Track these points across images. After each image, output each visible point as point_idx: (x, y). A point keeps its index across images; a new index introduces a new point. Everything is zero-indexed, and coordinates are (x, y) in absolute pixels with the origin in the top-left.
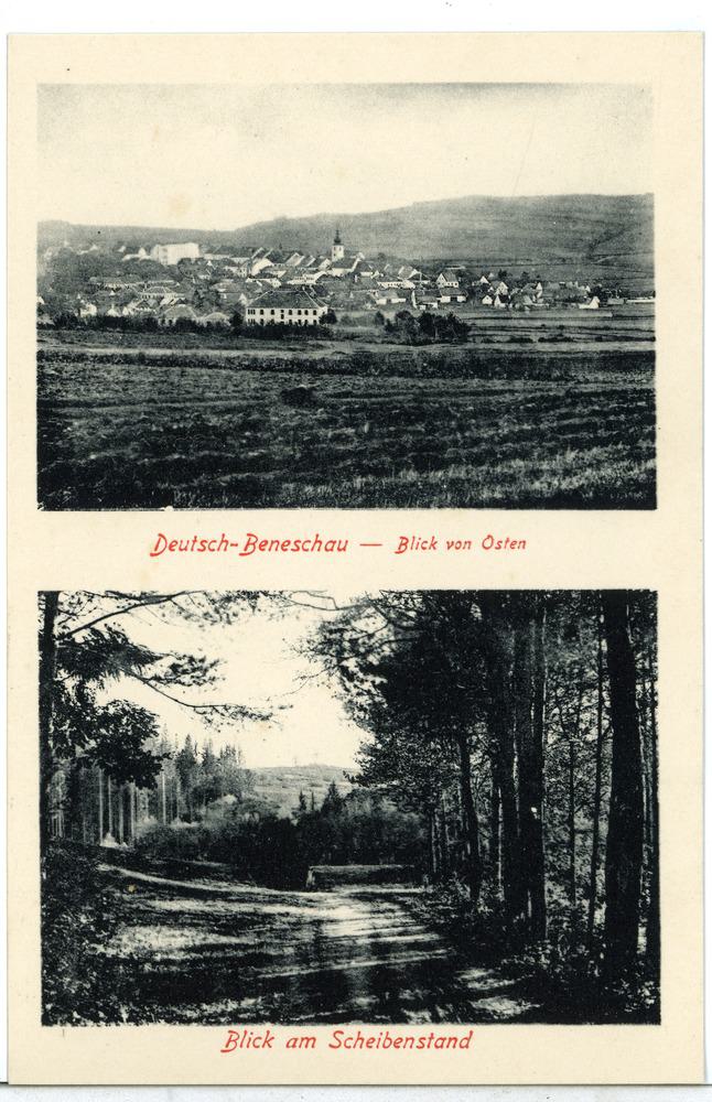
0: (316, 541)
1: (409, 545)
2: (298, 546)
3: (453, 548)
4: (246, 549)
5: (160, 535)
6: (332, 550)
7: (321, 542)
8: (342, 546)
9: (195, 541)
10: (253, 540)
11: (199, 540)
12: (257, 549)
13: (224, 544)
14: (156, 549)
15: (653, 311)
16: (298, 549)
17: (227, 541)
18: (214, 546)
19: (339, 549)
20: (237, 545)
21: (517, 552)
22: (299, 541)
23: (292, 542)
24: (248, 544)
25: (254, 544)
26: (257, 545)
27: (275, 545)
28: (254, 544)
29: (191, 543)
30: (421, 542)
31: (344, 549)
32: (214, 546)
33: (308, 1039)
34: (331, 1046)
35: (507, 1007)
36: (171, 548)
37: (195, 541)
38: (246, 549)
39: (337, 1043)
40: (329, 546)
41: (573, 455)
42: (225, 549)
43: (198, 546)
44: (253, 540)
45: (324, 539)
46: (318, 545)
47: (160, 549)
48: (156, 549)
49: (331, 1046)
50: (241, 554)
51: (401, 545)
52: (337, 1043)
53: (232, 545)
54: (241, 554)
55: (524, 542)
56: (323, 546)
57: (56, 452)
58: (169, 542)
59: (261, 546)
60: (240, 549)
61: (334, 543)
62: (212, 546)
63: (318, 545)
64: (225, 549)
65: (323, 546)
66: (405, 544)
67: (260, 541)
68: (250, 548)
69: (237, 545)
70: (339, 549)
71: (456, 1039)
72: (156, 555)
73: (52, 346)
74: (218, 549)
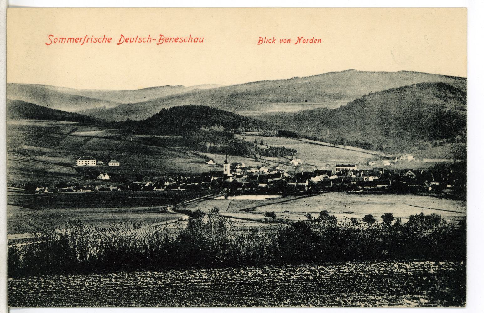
1: (263, 41)
2: (183, 40)
3: (283, 43)
5: (122, 35)
6: (197, 42)
7: (106, 38)
8: (201, 40)
9: (137, 38)
11: (139, 38)
14: (120, 41)
17: (151, 38)
20: (155, 40)
21: (318, 44)
22: (97, 38)
23: (180, 38)
24: (160, 39)
25: (163, 39)
26: (164, 40)
27: (172, 39)
29: (135, 39)
30: (268, 40)
31: (202, 41)
32: (145, 40)
35: (128, 93)
36: (283, 40)
37: (137, 38)
38: (159, 41)
39: (95, 41)
40: (196, 40)
42: (150, 42)
43: (138, 40)
45: (193, 37)
46: (191, 39)
48: (120, 41)
51: (260, 40)
52: (95, 41)
53: (153, 40)
54: (157, 44)
55: (321, 40)
56: (193, 39)
57: (57, 111)
58: (125, 39)
59: (166, 40)
61: (198, 38)
64: (150, 42)
65: (193, 39)
66: (262, 41)
67: (165, 38)
68: (161, 41)
69: (155, 40)
70: (200, 42)
71: (74, 39)
72: (160, 44)
73: (13, 237)
74: (188, 42)
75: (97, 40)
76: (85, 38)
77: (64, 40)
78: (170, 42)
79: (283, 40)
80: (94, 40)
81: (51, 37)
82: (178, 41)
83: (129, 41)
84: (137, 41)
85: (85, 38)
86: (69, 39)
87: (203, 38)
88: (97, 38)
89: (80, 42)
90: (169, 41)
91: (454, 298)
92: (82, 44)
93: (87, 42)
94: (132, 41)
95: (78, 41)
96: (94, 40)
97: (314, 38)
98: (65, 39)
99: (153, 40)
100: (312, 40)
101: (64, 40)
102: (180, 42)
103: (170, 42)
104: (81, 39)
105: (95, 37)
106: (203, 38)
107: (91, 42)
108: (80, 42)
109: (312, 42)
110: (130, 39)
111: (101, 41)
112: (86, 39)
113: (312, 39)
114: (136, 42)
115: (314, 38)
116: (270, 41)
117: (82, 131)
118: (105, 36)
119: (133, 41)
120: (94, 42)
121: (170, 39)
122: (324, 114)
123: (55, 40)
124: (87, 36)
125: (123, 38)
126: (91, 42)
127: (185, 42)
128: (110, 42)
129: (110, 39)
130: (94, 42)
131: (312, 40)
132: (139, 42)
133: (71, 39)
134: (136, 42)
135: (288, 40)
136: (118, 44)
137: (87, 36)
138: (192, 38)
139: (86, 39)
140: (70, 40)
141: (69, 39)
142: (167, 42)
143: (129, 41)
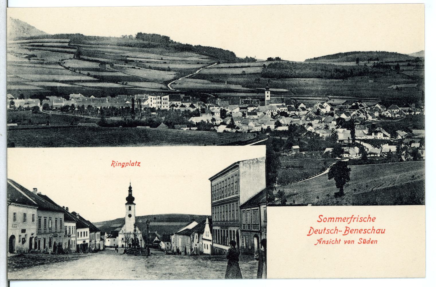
0: (369, 218)
4: (345, 233)
5: (311, 227)
6: (379, 233)
7: (371, 218)
8: (383, 232)
9: (325, 229)
10: (348, 229)
11: (327, 229)
12: (349, 232)
13: (336, 231)
14: (309, 232)
15: (424, 134)
16: (365, 230)
17: (337, 230)
18: (369, 231)
19: (382, 233)
20: (341, 231)
24: (346, 231)
25: (348, 231)
26: (349, 231)
28: (348, 231)
29: (323, 231)
31: (384, 233)
33: (331, 218)
34: (318, 221)
37: (325, 229)
38: (345, 233)
39: (320, 220)
40: (378, 231)
41: (143, 120)
42: (337, 233)
43: (326, 231)
44: (348, 229)
47: (310, 234)
48: (309, 232)
49: (318, 221)
50: (343, 235)
53: (339, 231)
54: (343, 235)
59: (351, 231)
60: (343, 233)
61: (380, 230)
62: (369, 231)
63: (337, 242)
64: (337, 233)
69: (341, 231)
71: (341, 218)
72: (345, 235)
75: (362, 219)
76: (351, 218)
77: (333, 219)
78: (354, 233)
79: (347, 241)
80: (359, 219)
81: (321, 217)
82: (362, 232)
83: (318, 232)
84: (325, 233)
85: (351, 218)
86: (337, 218)
87: (385, 230)
88: (362, 218)
89: (347, 221)
90: (353, 232)
91: (136, 247)
92: (348, 223)
93: (353, 221)
94: (320, 232)
95: (346, 220)
96: (359, 219)
97: (370, 239)
98: (334, 218)
99: (339, 231)
100: (369, 241)
101: (332, 219)
102: (364, 233)
103: (354, 233)
104: (348, 218)
105: (361, 217)
106: (385, 230)
107: (357, 221)
108: (347, 221)
109: (369, 243)
110: (319, 231)
111: (366, 221)
112: (353, 219)
113: (369, 240)
114: (324, 233)
115: (370, 239)
116: (333, 242)
117: (181, 229)
118: (369, 215)
119: (321, 233)
120: (360, 221)
121: (354, 230)
122: (64, 144)
123: (325, 220)
124: (353, 216)
125: (312, 229)
126: (357, 221)
127: (368, 233)
128: (374, 221)
129: (374, 219)
130: (360, 221)
131: (369, 241)
132: (327, 233)
133: (339, 218)
134: (324, 233)
135: (352, 241)
136: (308, 235)
137: (353, 216)
138: (374, 230)
139: (353, 219)
140: (330, 219)
141: (337, 218)
142: (352, 233)
143: (318, 232)
